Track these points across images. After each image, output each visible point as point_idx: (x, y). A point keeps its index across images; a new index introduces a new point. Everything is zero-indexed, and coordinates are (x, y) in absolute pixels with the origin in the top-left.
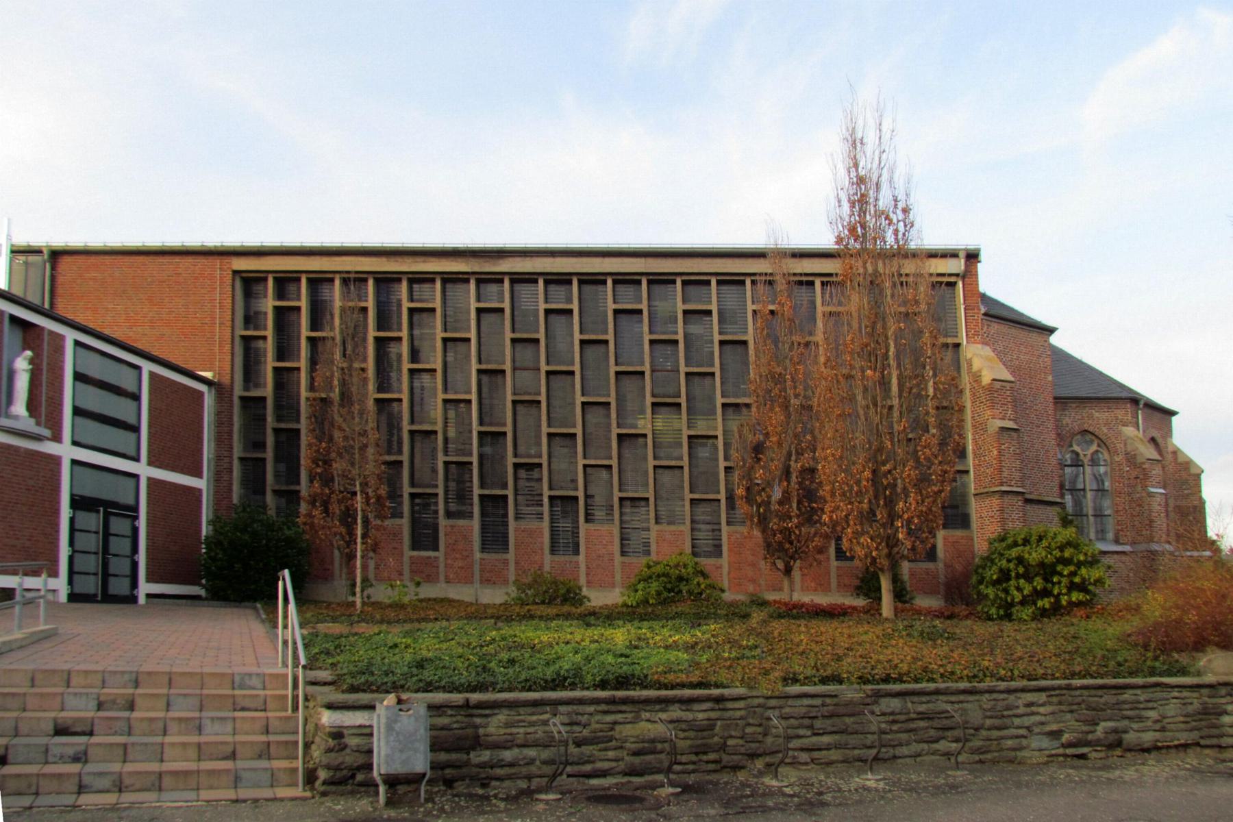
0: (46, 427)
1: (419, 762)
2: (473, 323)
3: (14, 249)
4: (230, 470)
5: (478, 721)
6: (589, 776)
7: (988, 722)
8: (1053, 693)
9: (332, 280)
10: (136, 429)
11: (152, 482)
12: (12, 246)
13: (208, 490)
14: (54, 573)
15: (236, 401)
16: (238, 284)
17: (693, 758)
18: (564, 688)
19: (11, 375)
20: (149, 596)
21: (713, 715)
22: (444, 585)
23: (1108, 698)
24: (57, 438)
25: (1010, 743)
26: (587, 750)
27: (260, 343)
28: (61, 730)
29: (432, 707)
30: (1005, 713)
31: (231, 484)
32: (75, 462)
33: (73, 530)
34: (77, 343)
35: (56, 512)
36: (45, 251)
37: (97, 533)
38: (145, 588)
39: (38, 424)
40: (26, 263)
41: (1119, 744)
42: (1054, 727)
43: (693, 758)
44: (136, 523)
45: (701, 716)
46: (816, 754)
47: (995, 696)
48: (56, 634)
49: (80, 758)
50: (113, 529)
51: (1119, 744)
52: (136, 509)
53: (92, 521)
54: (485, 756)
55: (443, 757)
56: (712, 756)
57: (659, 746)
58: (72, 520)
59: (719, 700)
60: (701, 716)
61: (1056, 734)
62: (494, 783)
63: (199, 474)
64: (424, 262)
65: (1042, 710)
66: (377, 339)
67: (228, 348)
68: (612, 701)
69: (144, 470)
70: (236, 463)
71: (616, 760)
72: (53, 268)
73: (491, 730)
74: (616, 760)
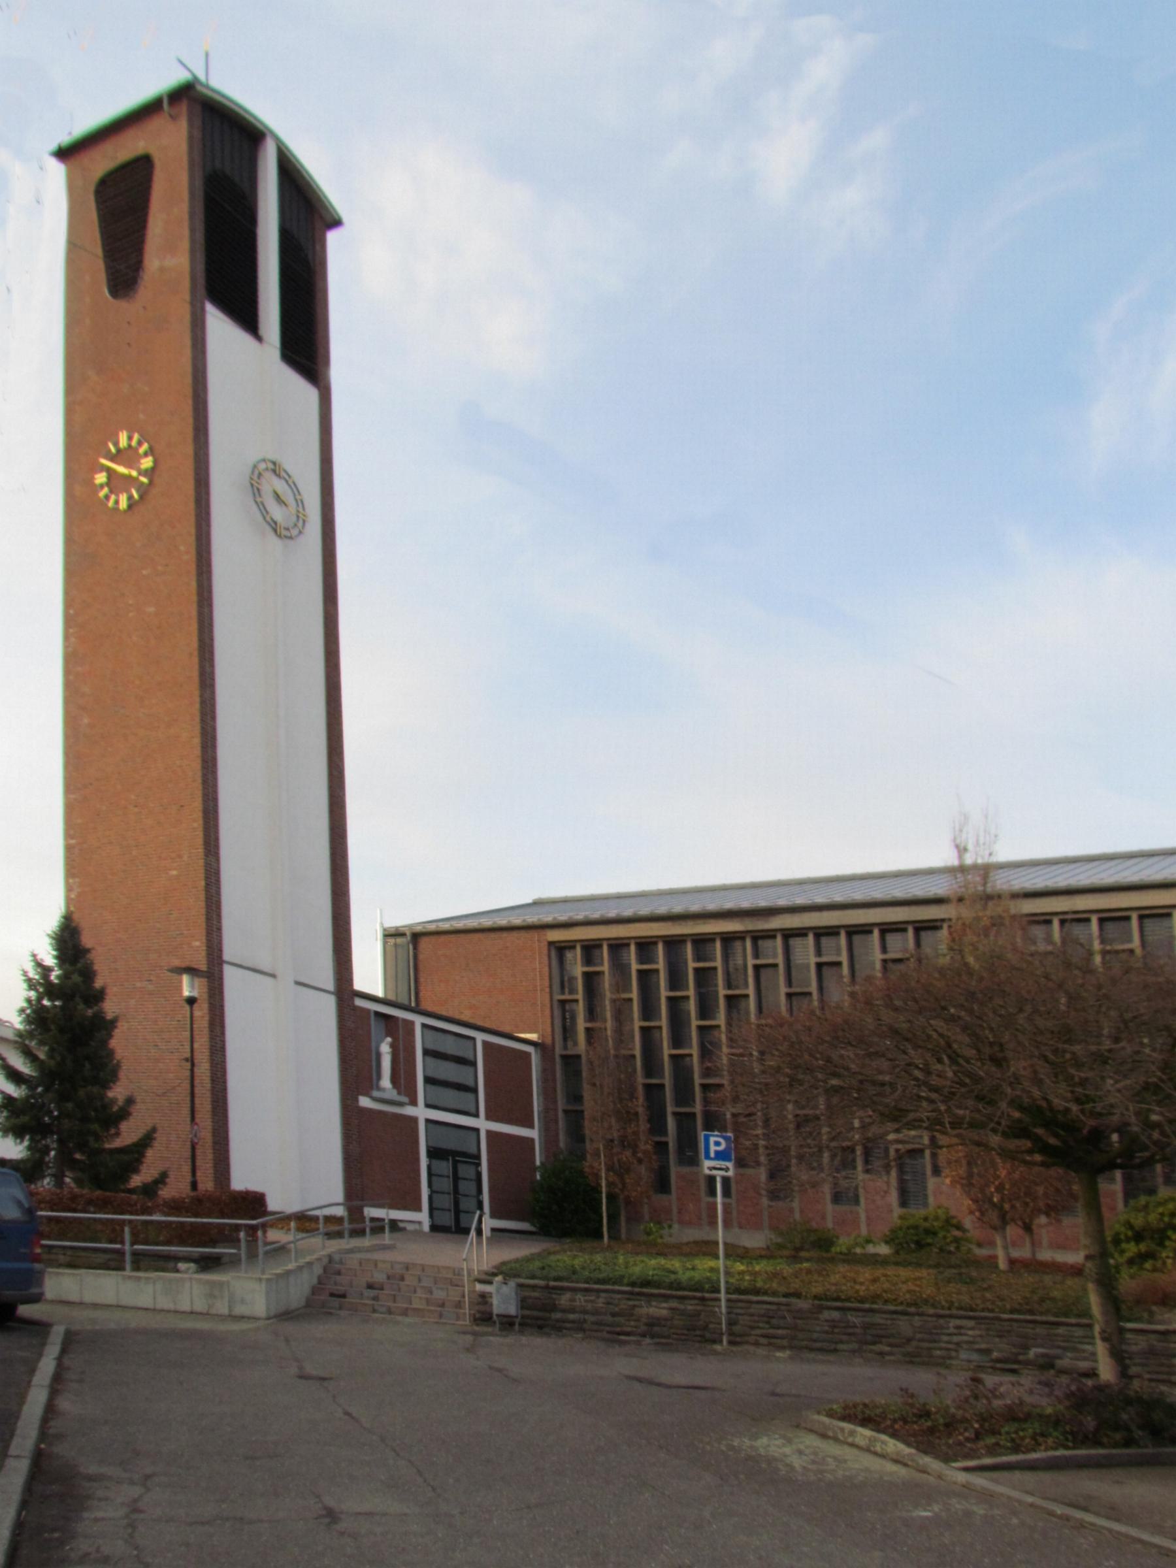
0: (406, 1095)
1: (512, 1310)
2: (751, 980)
3: (387, 933)
4: (556, 1122)
5: (554, 1296)
6: (619, 1334)
7: (919, 1336)
8: (983, 1321)
9: (628, 945)
10: (475, 1090)
11: (489, 1133)
12: (385, 930)
13: (540, 1138)
14: (418, 1209)
15: (558, 1059)
16: (553, 953)
17: (686, 1332)
18: (609, 1284)
19: (379, 1055)
20: (493, 1230)
21: (699, 1308)
22: (737, 1230)
23: (1040, 1330)
24: (414, 1102)
25: (938, 1353)
26: (617, 1319)
27: (574, 1006)
28: (370, 1286)
29: (520, 1286)
30: (934, 1331)
31: (557, 1135)
32: (428, 1121)
33: (430, 1174)
34: (424, 1026)
35: (417, 1160)
36: (408, 934)
37: (448, 1177)
38: (488, 1223)
39: (399, 1093)
40: (396, 945)
41: (1052, 1366)
42: (983, 1346)
43: (686, 1332)
44: (479, 1169)
45: (690, 1307)
46: (773, 1341)
47: (925, 1318)
48: (395, 1247)
49: (376, 1298)
50: (461, 1174)
51: (1052, 1366)
52: (478, 1157)
53: (445, 1167)
54: (558, 1315)
55: (527, 1312)
56: (698, 1333)
57: (663, 1322)
58: (429, 1168)
59: (703, 1299)
60: (690, 1307)
61: (987, 1352)
62: (564, 1331)
63: (530, 1125)
64: (704, 923)
65: (970, 1333)
66: (669, 999)
67: (548, 1012)
68: (631, 1293)
69: (483, 1124)
70: (561, 1115)
71: (636, 1327)
72: (415, 948)
73: (563, 1302)
74: (636, 1327)
